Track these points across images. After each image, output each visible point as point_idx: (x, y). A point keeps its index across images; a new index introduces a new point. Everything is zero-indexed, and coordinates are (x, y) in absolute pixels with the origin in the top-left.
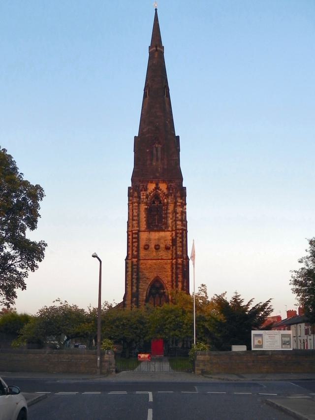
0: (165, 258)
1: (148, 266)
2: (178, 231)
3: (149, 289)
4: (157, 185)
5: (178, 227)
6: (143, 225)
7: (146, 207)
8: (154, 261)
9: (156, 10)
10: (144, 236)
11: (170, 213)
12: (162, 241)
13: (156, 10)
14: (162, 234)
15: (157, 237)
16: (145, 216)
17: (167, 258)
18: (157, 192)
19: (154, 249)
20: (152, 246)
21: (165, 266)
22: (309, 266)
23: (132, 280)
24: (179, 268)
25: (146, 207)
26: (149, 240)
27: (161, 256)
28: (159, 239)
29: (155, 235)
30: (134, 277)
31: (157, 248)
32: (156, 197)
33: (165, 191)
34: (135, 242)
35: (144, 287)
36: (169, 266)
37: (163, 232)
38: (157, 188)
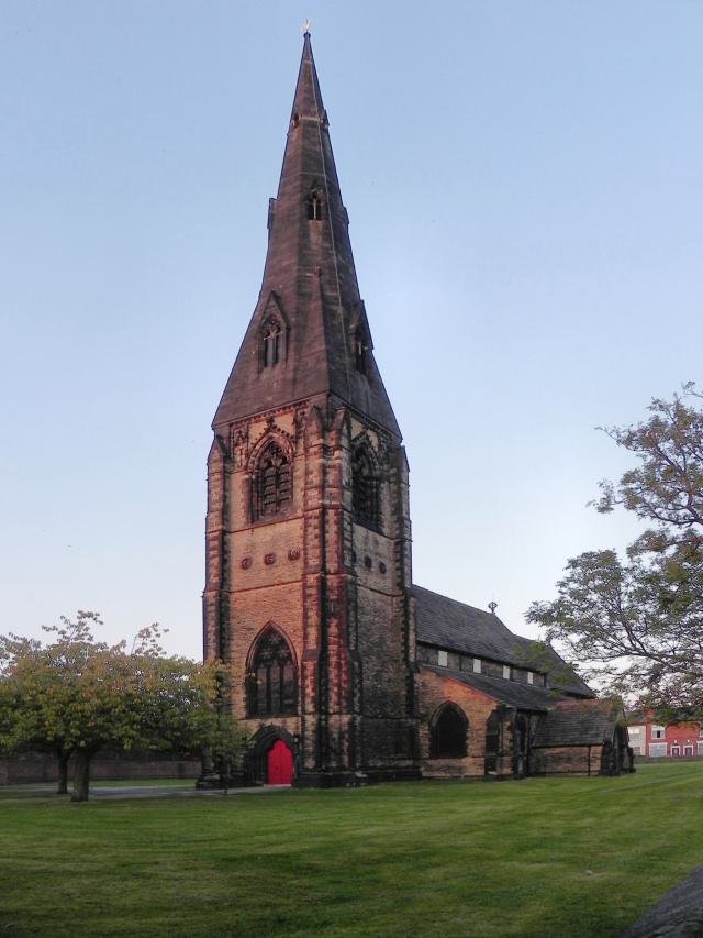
0: (288, 579)
1: (251, 603)
2: (310, 513)
3: (253, 652)
4: (270, 421)
5: (310, 503)
6: (239, 516)
7: (247, 477)
8: (263, 590)
9: (307, 36)
10: (239, 543)
11: (299, 478)
12: (282, 543)
13: (307, 36)
14: (282, 528)
15: (269, 538)
16: (242, 496)
17: (294, 579)
18: (271, 438)
19: (263, 565)
20: (259, 559)
21: (289, 597)
22: (332, 932)
23: (305, 629)
24: (310, 595)
25: (247, 477)
26: (253, 546)
27: (279, 576)
28: (274, 541)
29: (265, 535)
30: (210, 628)
31: (269, 560)
32: (272, 447)
33: (290, 430)
34: (214, 556)
35: (241, 648)
36: (298, 595)
37: (284, 524)
38: (272, 427)
